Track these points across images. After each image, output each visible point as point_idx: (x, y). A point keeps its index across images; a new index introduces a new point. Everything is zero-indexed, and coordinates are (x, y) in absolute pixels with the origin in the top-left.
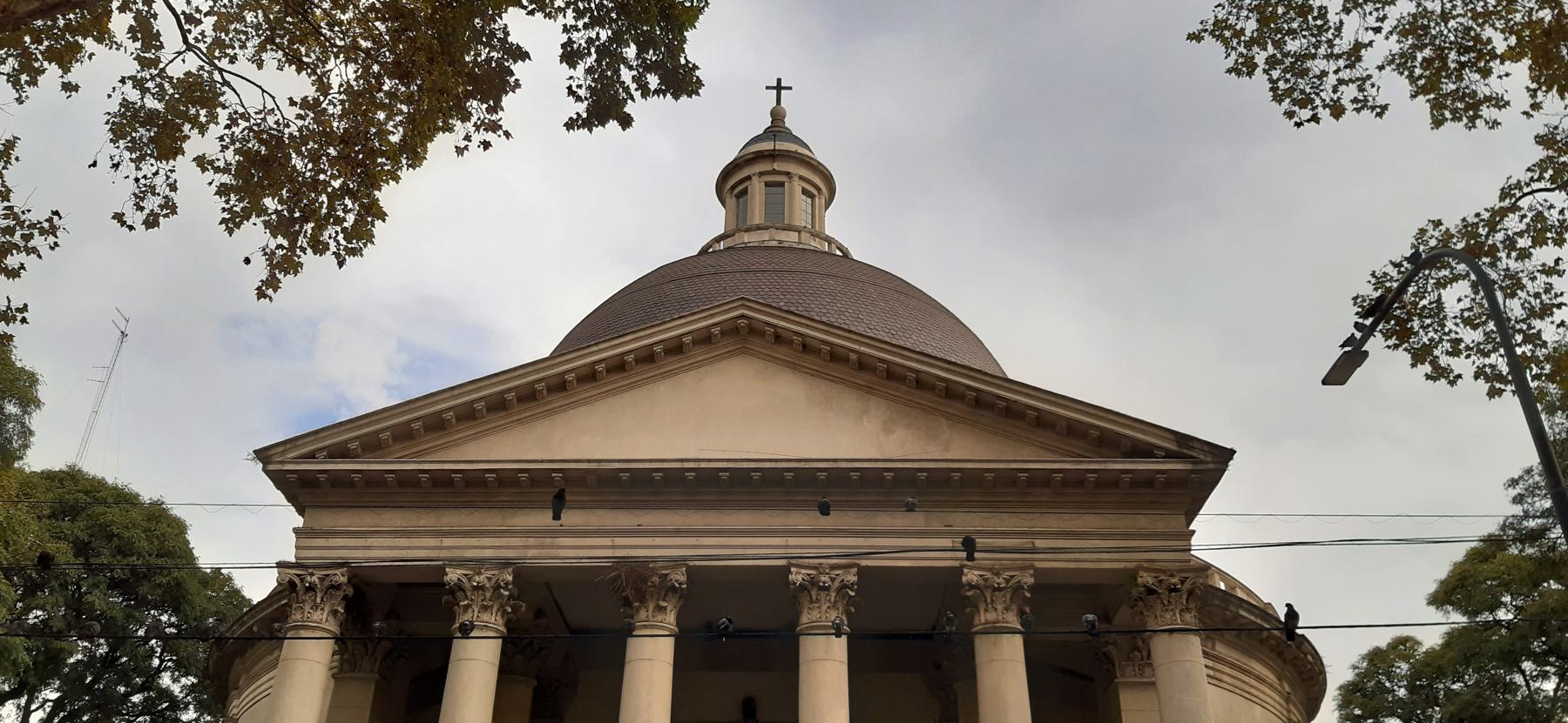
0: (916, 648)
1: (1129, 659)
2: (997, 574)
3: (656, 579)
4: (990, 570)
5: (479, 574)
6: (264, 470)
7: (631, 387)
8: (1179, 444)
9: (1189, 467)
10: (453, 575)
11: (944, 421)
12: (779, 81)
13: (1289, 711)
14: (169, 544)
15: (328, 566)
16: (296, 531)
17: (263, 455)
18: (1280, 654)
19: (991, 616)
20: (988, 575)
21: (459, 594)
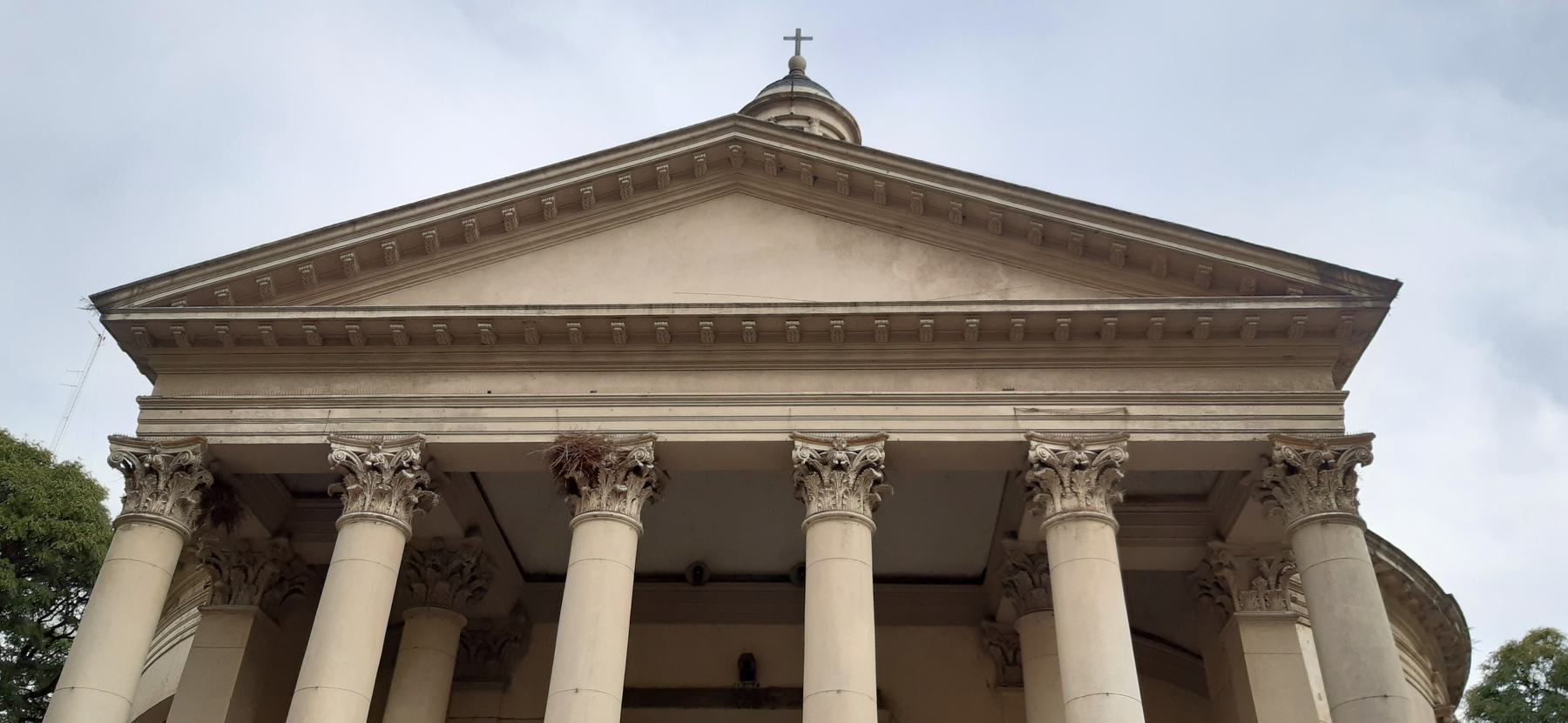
0: (966, 592)
1: (1251, 587)
2: (1078, 448)
3: (612, 458)
4: (1067, 443)
5: (376, 451)
6: (103, 322)
7: (591, 231)
8: (1323, 278)
9: (1339, 305)
10: (340, 453)
11: (1000, 267)
12: (798, 31)
13: (1435, 692)
14: (74, 506)
15: (176, 444)
16: (142, 401)
17: (102, 302)
18: (1422, 619)
19: (1070, 503)
20: (1065, 450)
21: (349, 478)
